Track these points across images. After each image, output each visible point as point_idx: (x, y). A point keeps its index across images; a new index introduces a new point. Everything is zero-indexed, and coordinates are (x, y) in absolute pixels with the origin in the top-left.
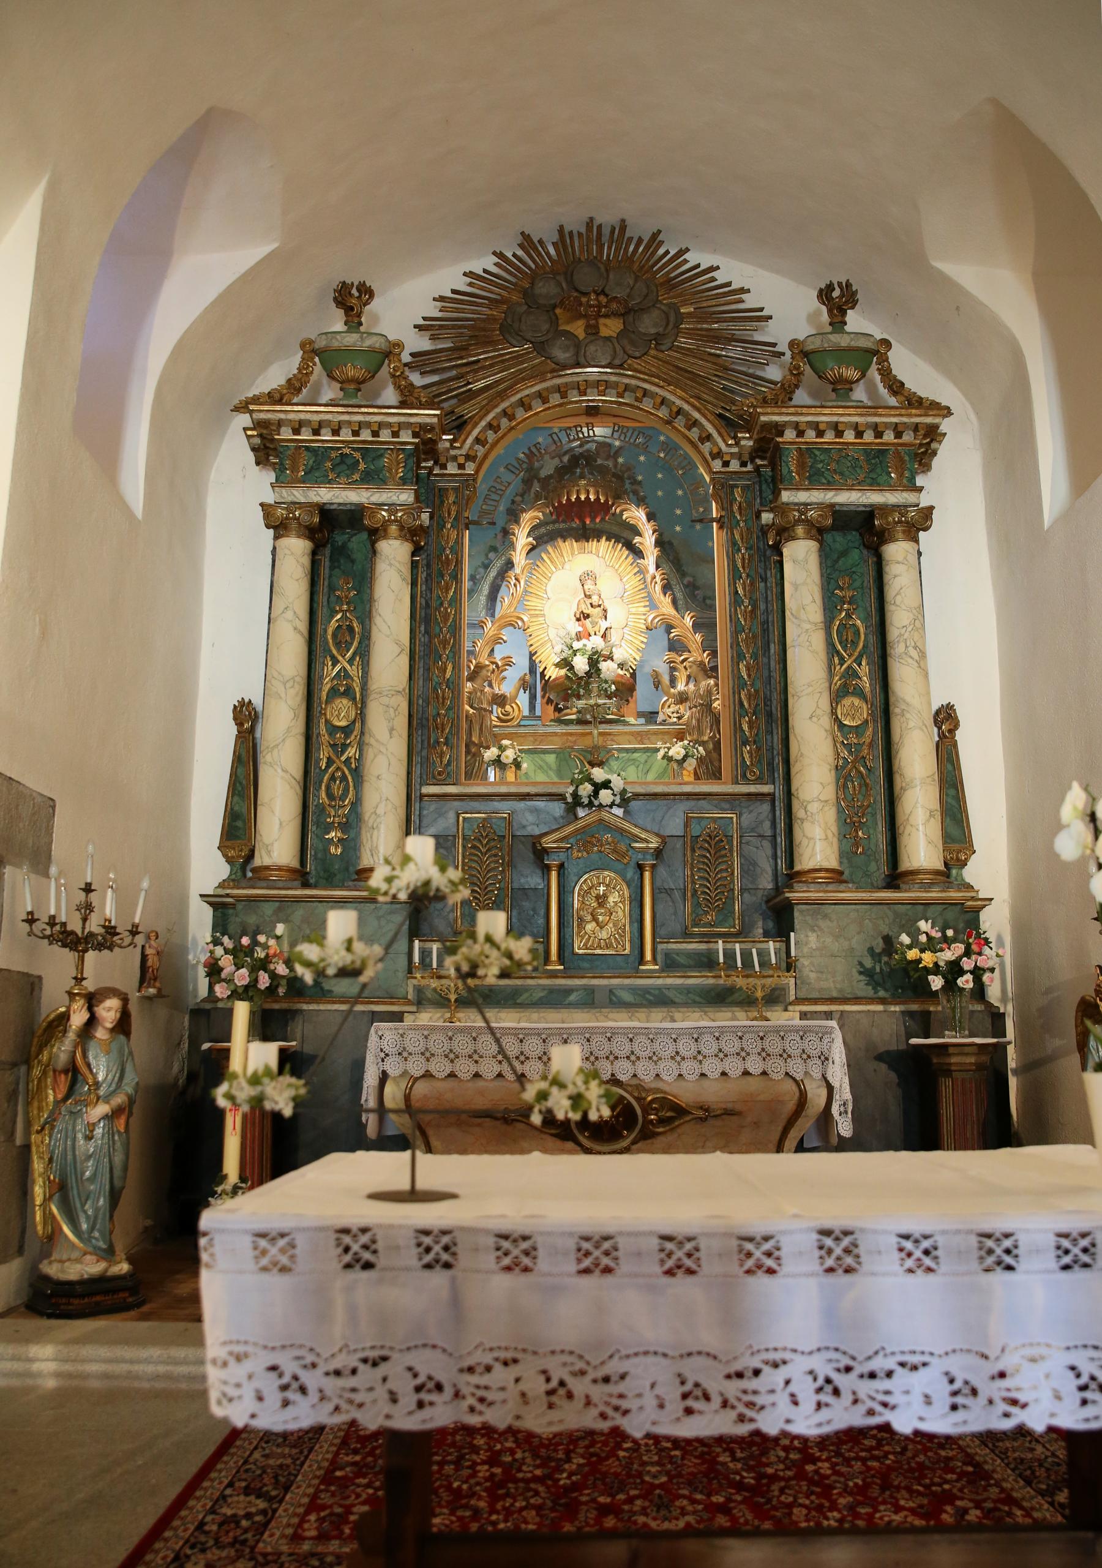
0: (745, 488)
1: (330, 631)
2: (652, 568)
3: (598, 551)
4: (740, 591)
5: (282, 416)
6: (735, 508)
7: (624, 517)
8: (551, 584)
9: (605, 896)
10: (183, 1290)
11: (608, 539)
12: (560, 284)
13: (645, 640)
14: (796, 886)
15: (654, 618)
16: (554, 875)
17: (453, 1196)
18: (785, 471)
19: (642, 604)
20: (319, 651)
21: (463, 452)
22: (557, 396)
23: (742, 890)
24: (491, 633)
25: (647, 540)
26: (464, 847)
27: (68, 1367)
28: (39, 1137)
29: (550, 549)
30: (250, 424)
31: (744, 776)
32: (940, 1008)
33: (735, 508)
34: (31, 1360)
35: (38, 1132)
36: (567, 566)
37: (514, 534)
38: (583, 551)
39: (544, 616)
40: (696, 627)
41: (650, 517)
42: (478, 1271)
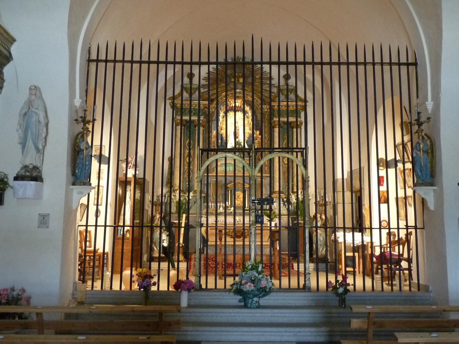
0: (268, 115)
1: (187, 143)
4: (266, 136)
5: (178, 102)
6: (266, 119)
9: (239, 196)
10: (3, 66)
12: (232, 71)
14: (274, 194)
16: (230, 191)
17: (270, 43)
18: (275, 114)
20: (185, 147)
21: (212, 107)
22: (231, 94)
23: (265, 194)
26: (213, 186)
27: (127, 261)
30: (171, 102)
31: (266, 172)
33: (266, 119)
40: (260, 134)
42: (234, 224)
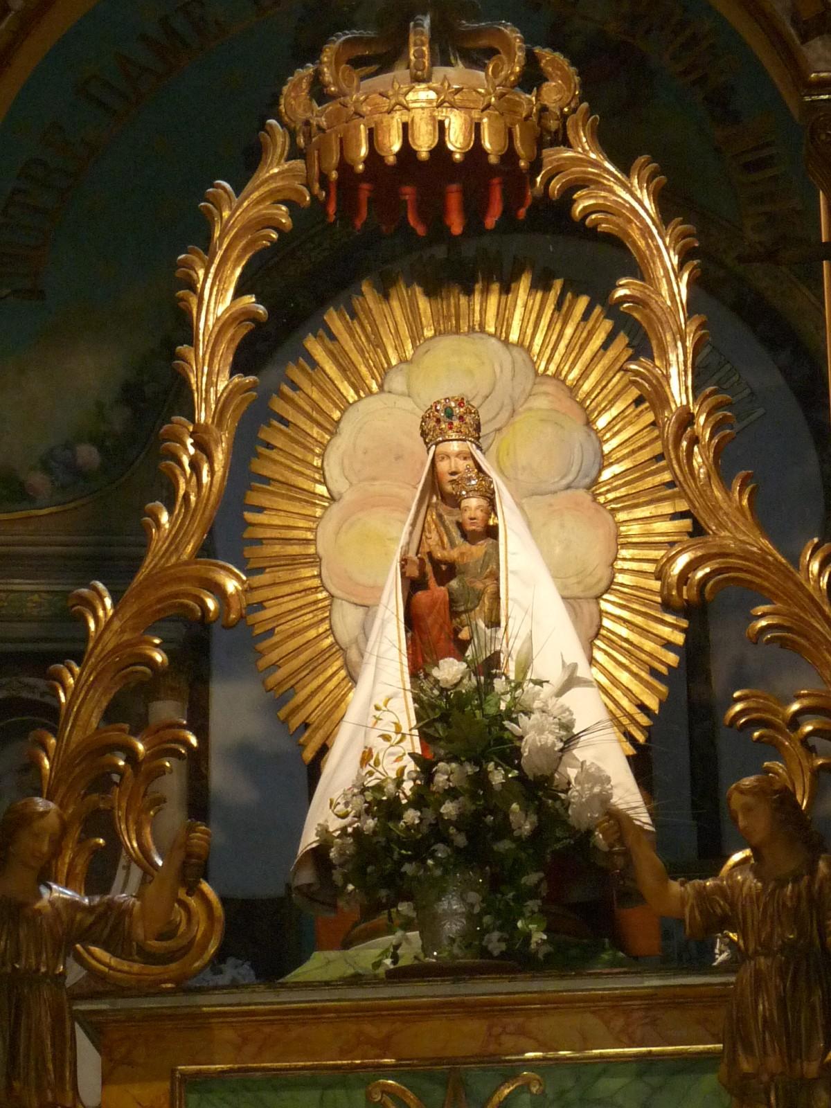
2: (679, 391)
3: (503, 320)
7: (578, 209)
8: (341, 444)
11: (541, 283)
13: (679, 638)
15: (692, 566)
19: (667, 508)
24: (110, 641)
25: (671, 283)
28: (339, 801)
29: (334, 319)
32: (346, 909)
34: (641, 291)
35: (339, 803)
36: (397, 382)
37: (191, 285)
38: (450, 326)
39: (316, 560)
41: (670, 204)
